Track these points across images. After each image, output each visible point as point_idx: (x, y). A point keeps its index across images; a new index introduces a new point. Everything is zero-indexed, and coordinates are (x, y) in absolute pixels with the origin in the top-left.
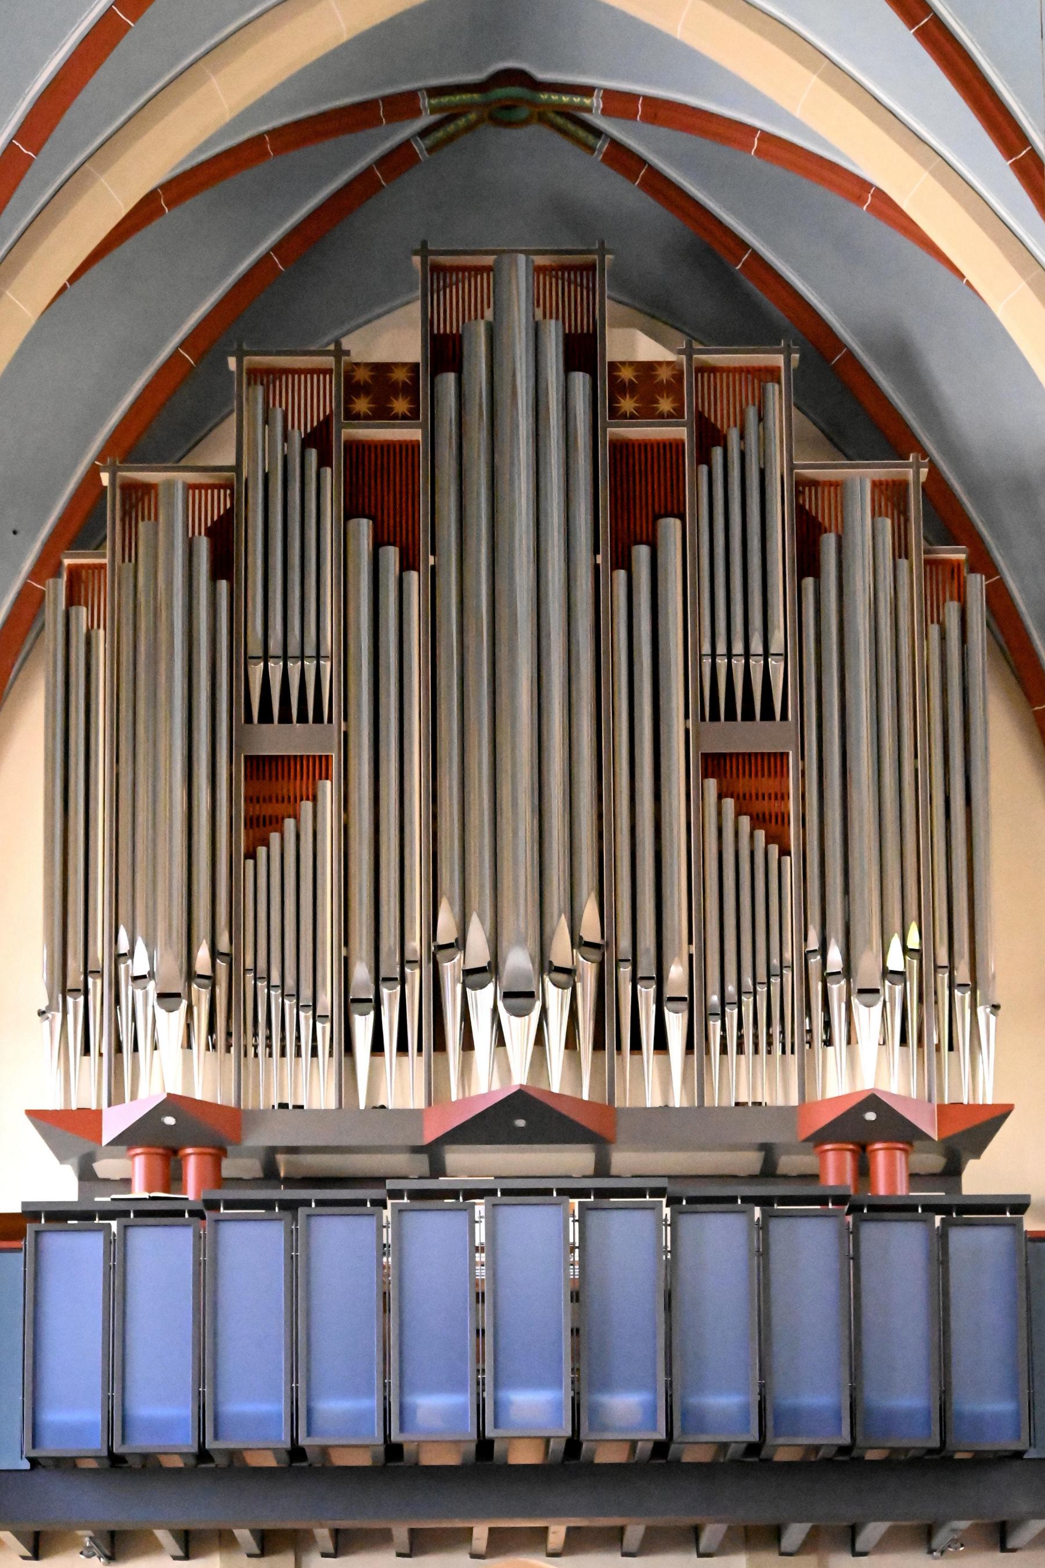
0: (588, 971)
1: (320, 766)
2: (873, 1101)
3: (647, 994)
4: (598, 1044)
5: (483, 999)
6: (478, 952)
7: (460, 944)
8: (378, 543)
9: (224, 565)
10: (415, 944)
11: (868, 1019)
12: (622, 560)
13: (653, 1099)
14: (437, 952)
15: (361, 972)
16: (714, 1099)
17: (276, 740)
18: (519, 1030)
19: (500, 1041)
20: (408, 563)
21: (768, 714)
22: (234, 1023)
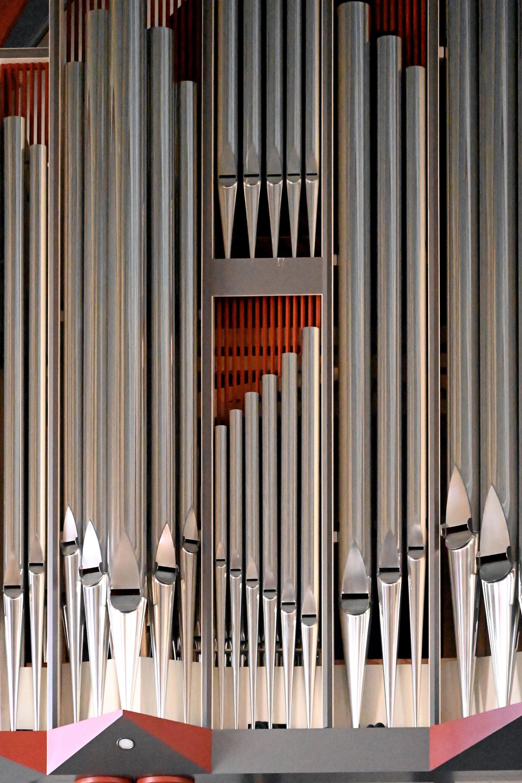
1: (305, 309)
7: (474, 526)
8: (376, 32)
9: (189, 64)
10: (418, 527)
12: (223, 420)
14: (446, 536)
15: (355, 563)
16: (269, 178)
17: (253, 278)
20: (412, 56)
21: (304, 251)
22: (202, 623)
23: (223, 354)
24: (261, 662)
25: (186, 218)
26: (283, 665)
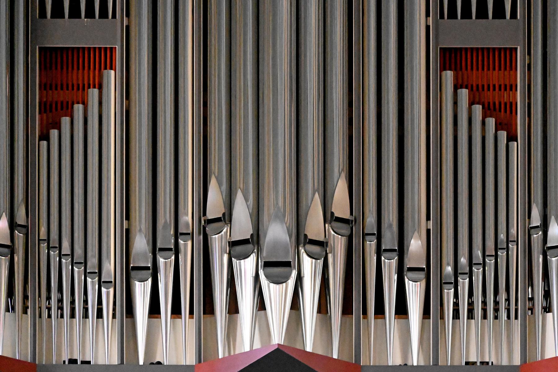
0: (339, 244)
1: (105, 57)
3: (390, 264)
4: (347, 310)
5: (247, 267)
6: (242, 224)
7: (227, 218)
13: (395, 359)
15: (141, 244)
16: (450, 357)
17: (67, 34)
18: (277, 295)
19: (261, 305)
20: (512, 137)
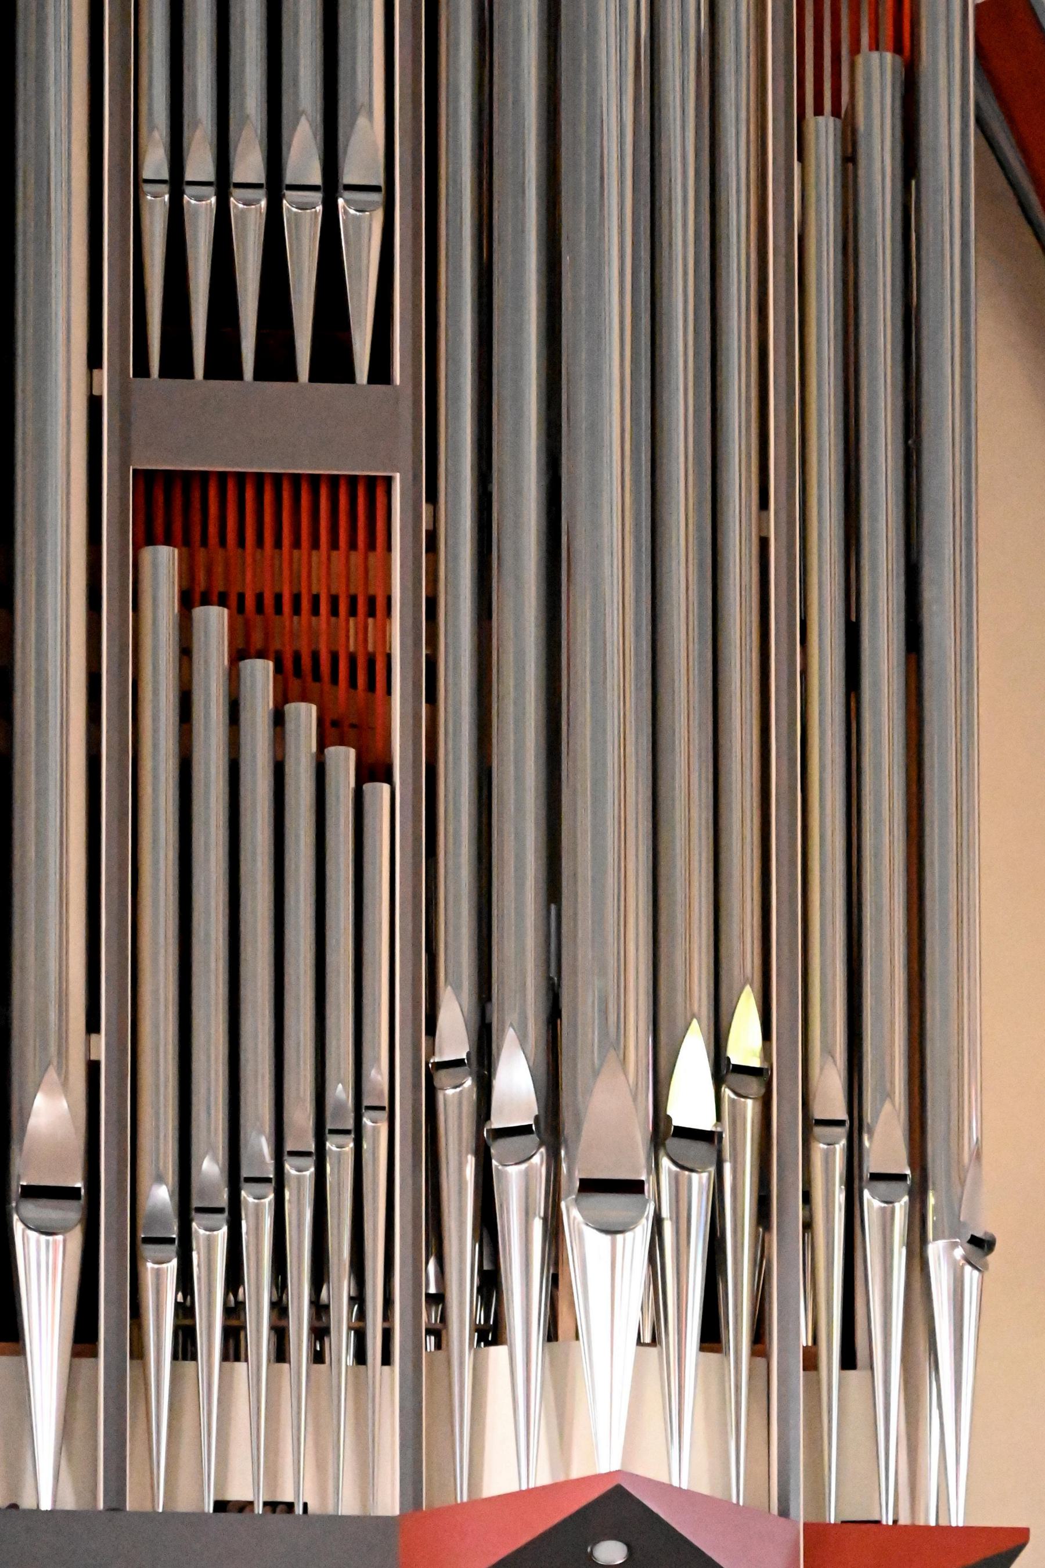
2: (616, 1508)
11: (609, 1268)
16: (152, 1490)
21: (331, 363)
23: (371, 601)
24: (281, 1354)
25: (598, 278)
26: (194, 1358)
